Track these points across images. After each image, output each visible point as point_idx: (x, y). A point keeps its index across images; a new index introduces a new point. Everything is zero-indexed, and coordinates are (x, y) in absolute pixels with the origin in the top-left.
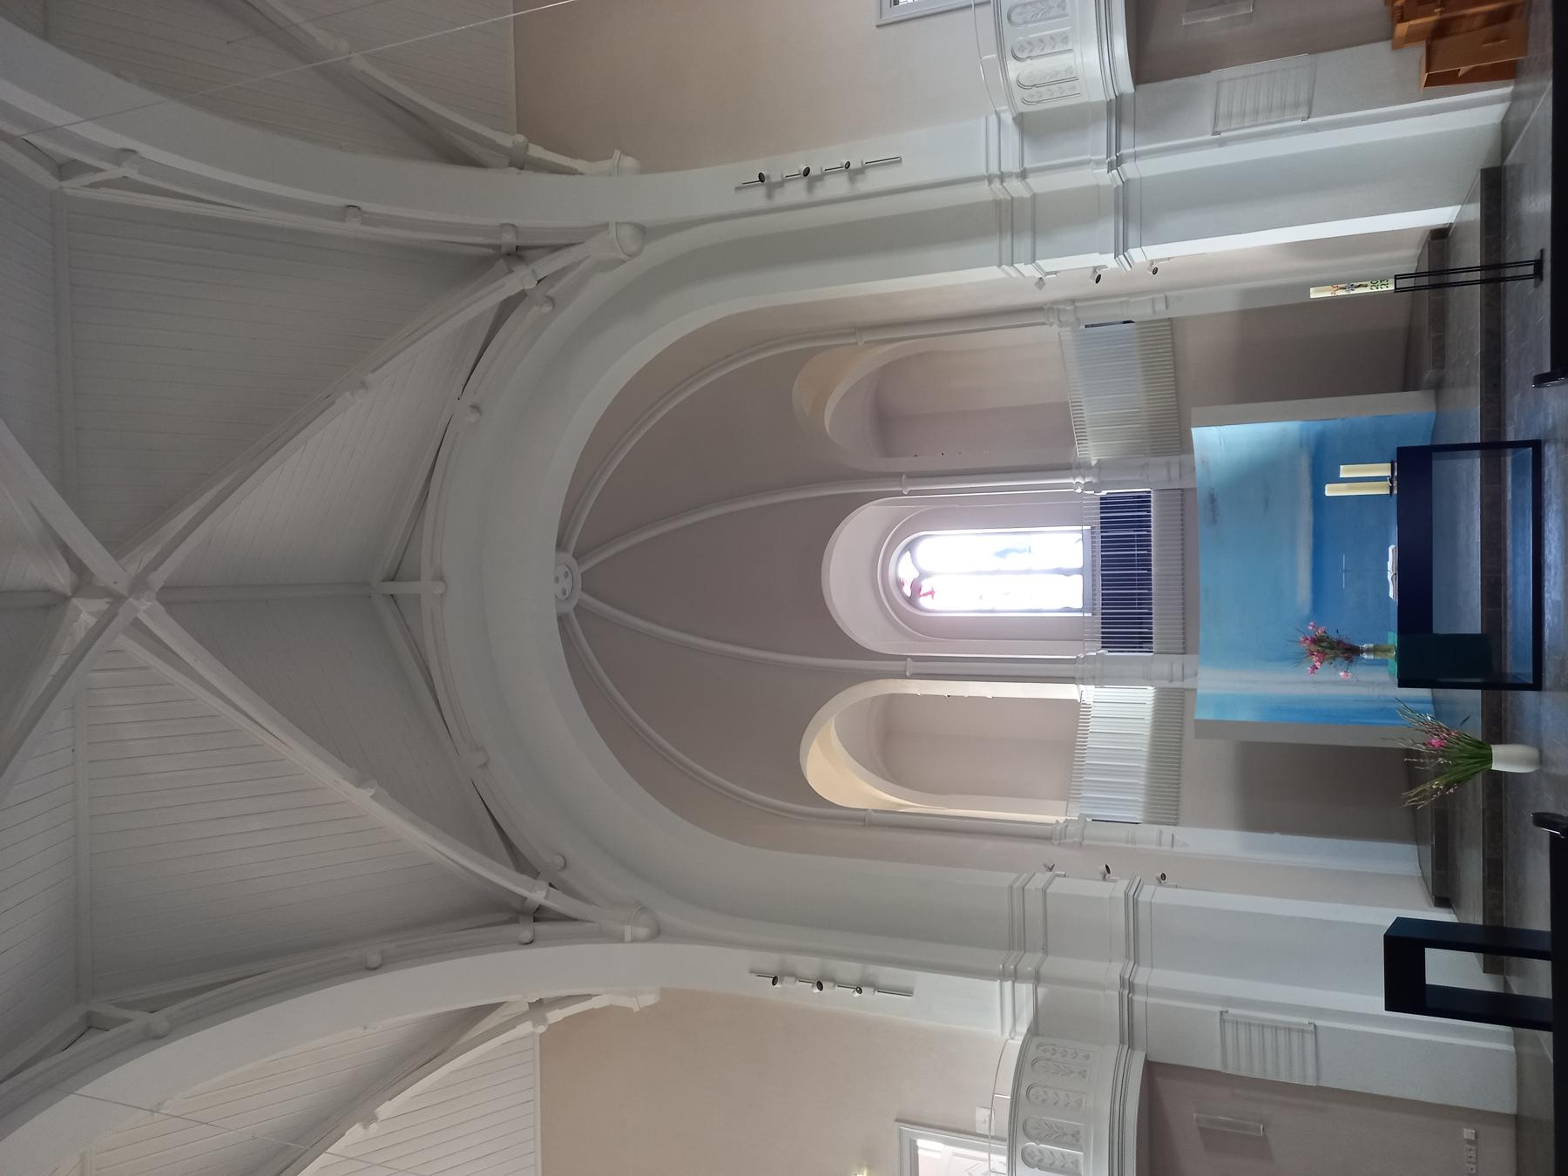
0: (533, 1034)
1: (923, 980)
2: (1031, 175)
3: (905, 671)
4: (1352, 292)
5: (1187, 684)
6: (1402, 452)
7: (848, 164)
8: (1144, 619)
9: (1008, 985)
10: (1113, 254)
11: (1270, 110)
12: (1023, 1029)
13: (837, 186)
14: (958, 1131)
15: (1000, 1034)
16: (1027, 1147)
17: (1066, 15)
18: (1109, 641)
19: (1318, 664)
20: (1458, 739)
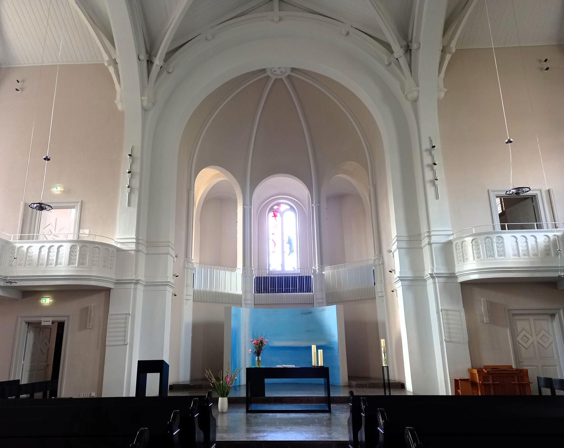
0: (103, 60)
1: (134, 210)
2: (429, 246)
3: (246, 205)
4: (383, 353)
5: (243, 305)
6: (327, 369)
7: (437, 180)
8: (266, 291)
9: (134, 241)
10: (399, 276)
11: (448, 324)
12: (119, 246)
13: (429, 176)
14: (80, 224)
15: (116, 238)
16: (77, 246)
17: (487, 258)
18: (258, 280)
19: (254, 342)
20: (229, 387)
